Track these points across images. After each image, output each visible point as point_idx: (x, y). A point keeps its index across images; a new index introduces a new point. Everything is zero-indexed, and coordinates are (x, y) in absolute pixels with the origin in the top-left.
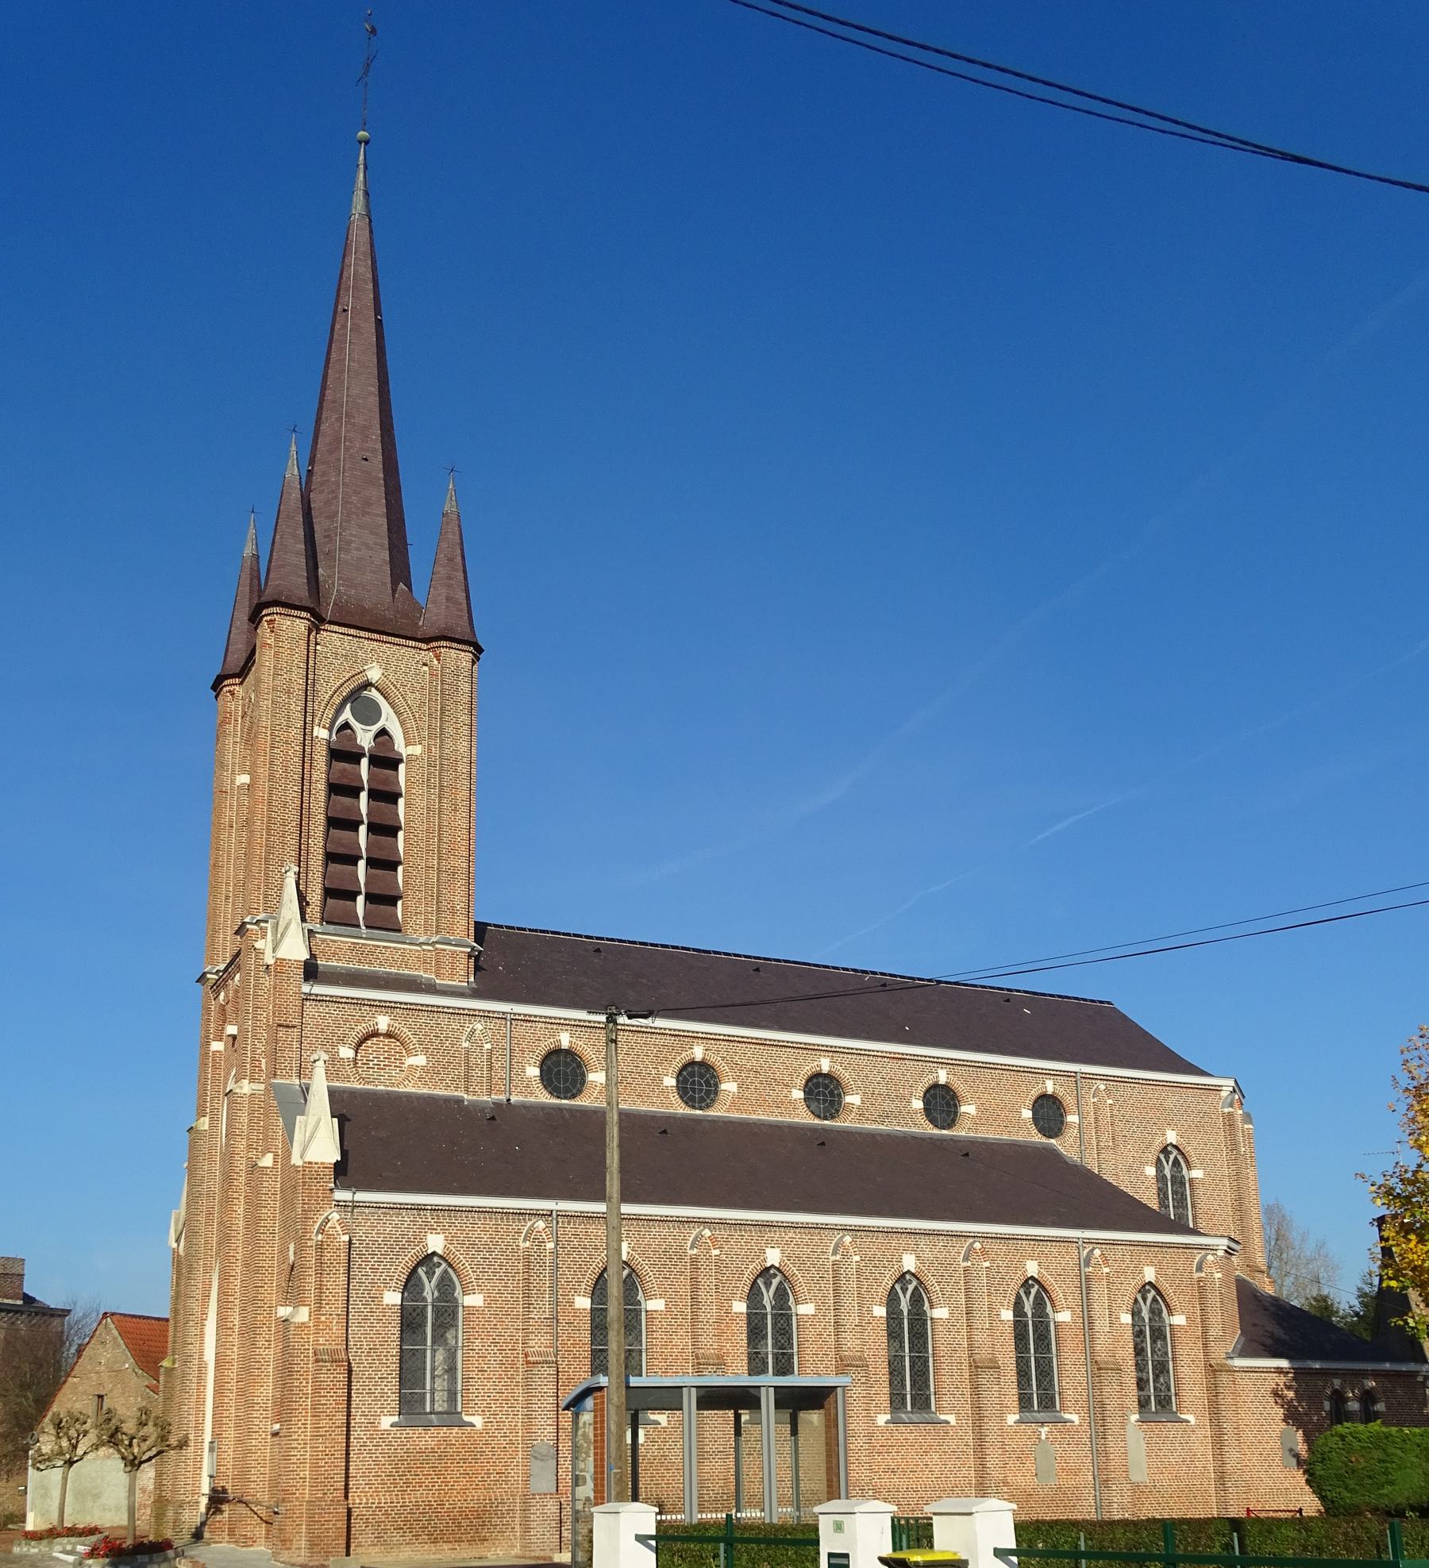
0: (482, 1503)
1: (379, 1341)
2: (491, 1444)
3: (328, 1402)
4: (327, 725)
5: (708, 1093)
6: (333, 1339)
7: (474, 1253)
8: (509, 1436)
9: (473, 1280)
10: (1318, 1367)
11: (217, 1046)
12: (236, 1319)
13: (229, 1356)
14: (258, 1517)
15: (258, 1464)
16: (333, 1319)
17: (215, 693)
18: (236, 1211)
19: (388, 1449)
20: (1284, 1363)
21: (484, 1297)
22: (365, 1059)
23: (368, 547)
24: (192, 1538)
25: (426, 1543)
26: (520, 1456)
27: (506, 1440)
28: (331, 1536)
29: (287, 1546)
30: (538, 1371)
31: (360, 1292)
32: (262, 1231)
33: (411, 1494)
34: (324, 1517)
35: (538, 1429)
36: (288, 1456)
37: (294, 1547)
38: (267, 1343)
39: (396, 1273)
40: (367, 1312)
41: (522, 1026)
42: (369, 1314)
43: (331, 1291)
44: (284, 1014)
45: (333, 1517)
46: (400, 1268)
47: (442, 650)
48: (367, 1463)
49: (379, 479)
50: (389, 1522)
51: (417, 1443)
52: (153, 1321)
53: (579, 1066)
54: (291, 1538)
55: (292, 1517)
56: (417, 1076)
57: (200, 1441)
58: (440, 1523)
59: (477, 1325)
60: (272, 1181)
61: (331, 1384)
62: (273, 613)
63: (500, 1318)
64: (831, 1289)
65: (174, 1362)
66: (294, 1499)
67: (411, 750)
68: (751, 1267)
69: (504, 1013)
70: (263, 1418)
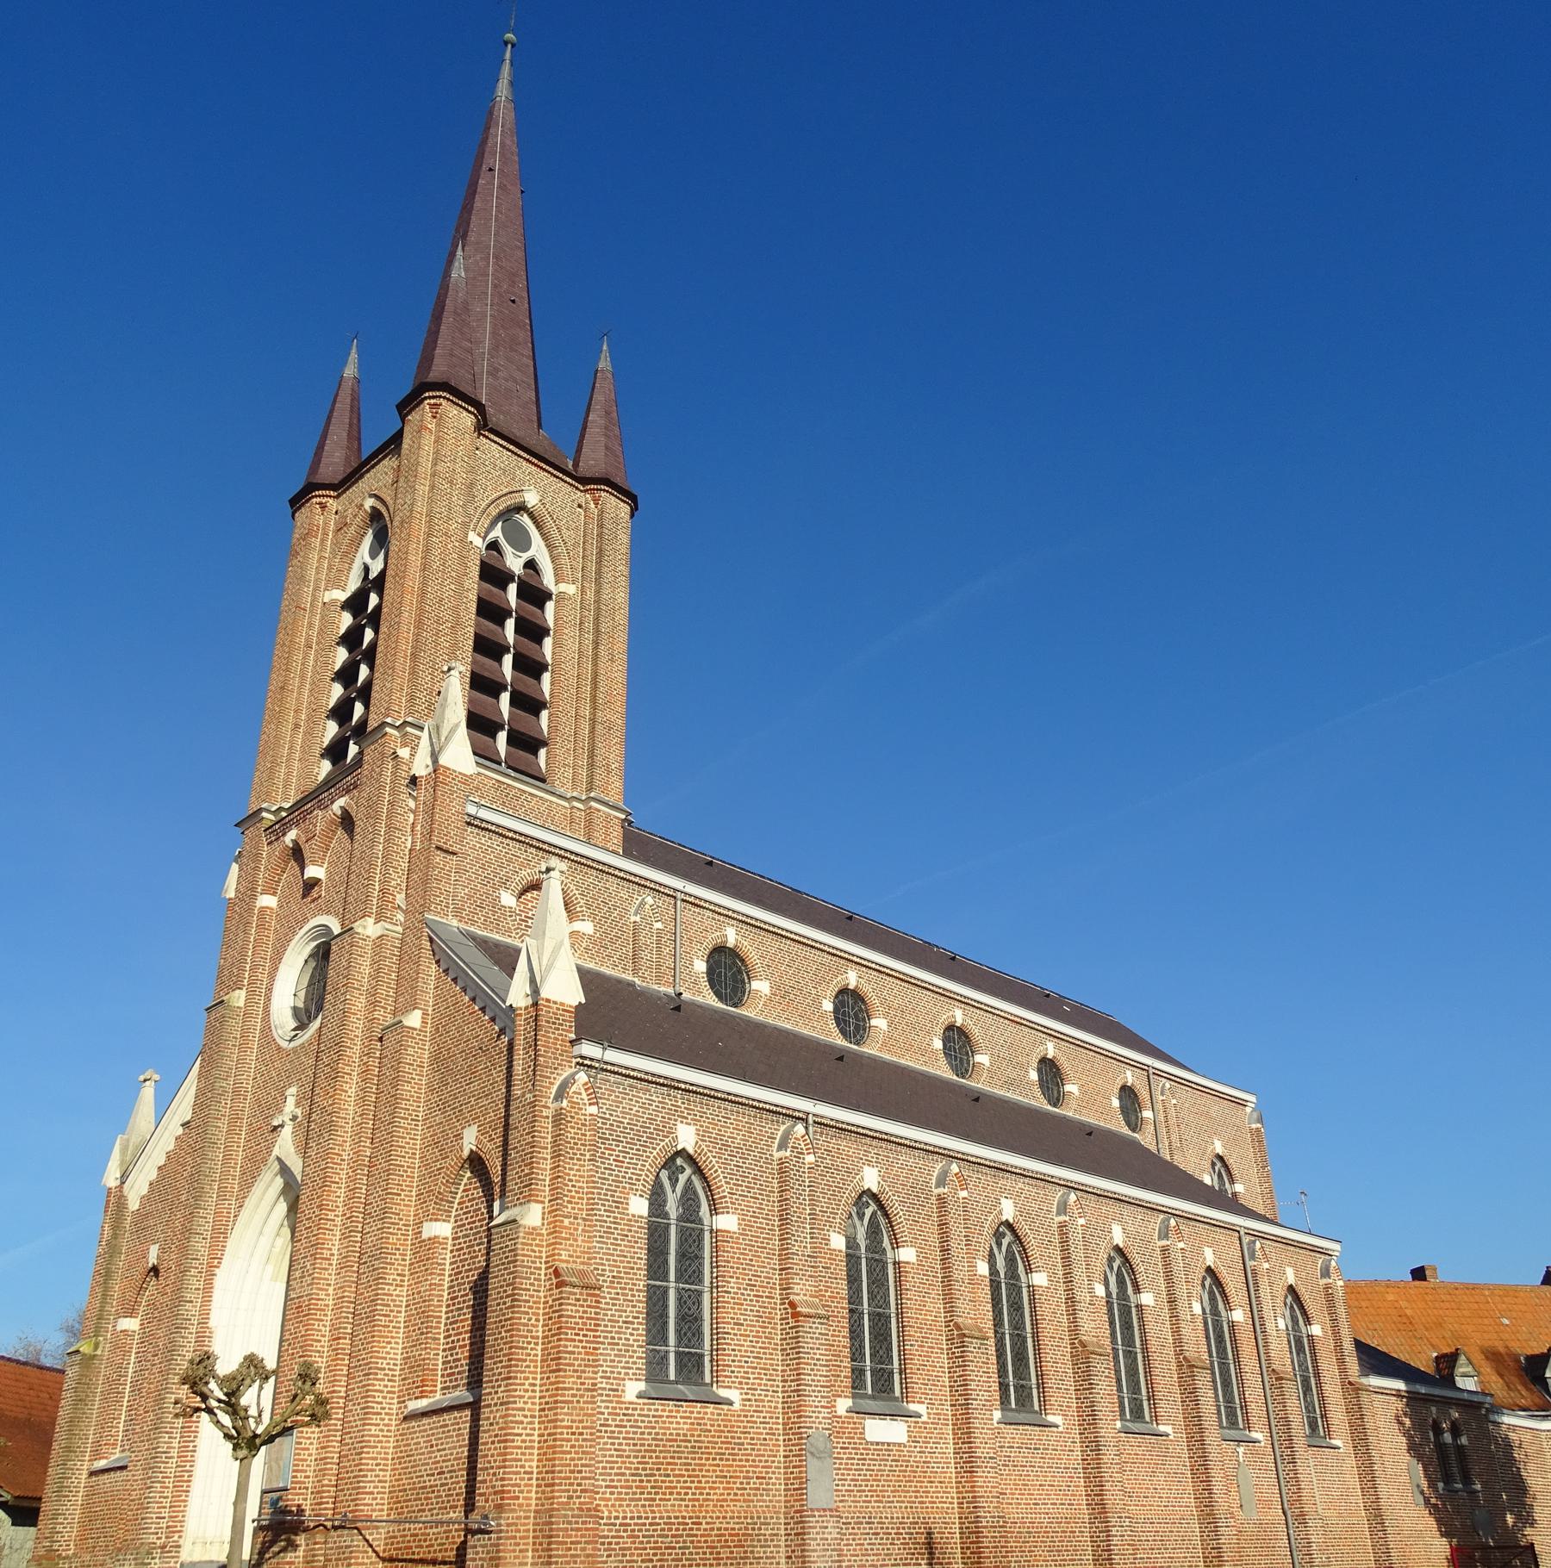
0: (743, 1523)
3: (576, 1350)
6: (579, 1254)
9: (726, 1194)
10: (1423, 1392)
11: (268, 901)
13: (322, 1300)
15: (377, 1465)
20: (1401, 1385)
22: (523, 914)
23: (515, 381)
30: (811, 1327)
34: (571, 1536)
36: (506, 1435)
38: (399, 1278)
42: (613, 1226)
45: (582, 1536)
46: (647, 1164)
47: (603, 494)
48: (608, 1453)
51: (667, 1425)
53: (740, 972)
55: (515, 1537)
57: (191, 1448)
61: (580, 1321)
62: (440, 397)
65: (96, 1347)
67: (563, 587)
68: (990, 1219)
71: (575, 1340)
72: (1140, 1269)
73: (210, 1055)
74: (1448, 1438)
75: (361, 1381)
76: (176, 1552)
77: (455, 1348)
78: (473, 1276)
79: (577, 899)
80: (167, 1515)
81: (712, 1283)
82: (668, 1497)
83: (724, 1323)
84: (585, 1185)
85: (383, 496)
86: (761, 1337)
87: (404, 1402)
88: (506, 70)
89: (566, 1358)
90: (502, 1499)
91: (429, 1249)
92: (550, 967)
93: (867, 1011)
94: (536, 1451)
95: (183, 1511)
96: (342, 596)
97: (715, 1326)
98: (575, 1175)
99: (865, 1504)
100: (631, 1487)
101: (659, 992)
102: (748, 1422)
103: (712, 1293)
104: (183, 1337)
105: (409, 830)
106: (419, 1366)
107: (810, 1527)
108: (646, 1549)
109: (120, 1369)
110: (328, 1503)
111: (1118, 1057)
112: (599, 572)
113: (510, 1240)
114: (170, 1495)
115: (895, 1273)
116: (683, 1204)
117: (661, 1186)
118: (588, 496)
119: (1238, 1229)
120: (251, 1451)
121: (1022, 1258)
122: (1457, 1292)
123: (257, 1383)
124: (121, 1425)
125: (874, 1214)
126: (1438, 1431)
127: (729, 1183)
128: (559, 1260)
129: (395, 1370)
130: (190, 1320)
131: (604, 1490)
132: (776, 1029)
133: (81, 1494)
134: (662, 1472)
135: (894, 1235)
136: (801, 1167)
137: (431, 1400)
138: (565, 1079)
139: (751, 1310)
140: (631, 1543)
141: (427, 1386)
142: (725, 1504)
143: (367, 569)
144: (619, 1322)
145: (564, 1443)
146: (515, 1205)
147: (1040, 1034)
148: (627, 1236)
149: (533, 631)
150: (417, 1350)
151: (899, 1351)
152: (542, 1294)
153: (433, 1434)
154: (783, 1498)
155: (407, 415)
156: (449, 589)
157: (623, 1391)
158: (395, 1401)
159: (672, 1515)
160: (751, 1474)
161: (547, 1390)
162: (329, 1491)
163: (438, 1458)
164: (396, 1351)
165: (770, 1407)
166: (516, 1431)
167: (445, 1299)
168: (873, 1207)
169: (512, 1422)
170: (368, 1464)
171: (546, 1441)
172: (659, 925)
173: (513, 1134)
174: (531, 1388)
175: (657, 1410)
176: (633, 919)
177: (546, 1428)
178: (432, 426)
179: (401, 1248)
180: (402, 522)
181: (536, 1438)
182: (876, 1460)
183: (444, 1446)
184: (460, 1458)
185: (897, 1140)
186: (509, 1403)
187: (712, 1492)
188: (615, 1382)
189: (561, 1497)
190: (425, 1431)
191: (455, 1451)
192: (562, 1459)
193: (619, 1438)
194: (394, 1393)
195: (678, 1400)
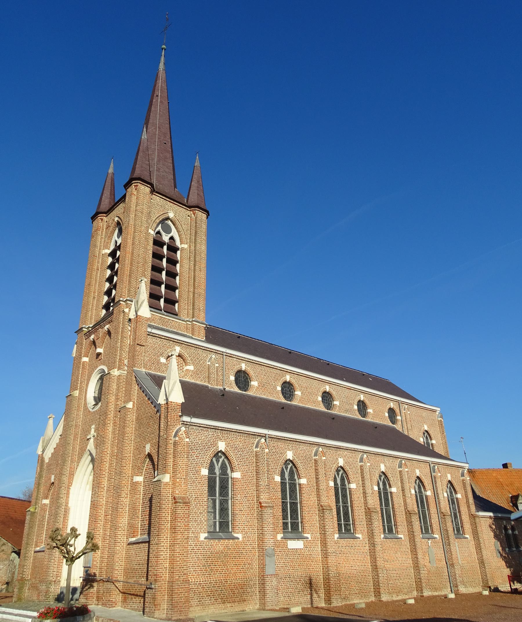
0: (243, 580)
3: (181, 525)
4: (154, 230)
5: (290, 395)
6: (182, 491)
8: (252, 545)
11: (85, 359)
12: (105, 483)
13: (101, 502)
14: (119, 590)
15: (119, 560)
16: (182, 481)
18: (109, 430)
20: (491, 514)
23: (166, 172)
24: (55, 601)
25: (220, 603)
26: (257, 555)
28: (183, 601)
29: (158, 608)
30: (267, 511)
32: (126, 439)
33: (213, 576)
34: (180, 590)
36: (158, 555)
37: (161, 608)
38: (126, 495)
39: (206, 459)
41: (228, 358)
42: (195, 479)
43: (181, 466)
45: (184, 590)
46: (208, 457)
47: (196, 211)
48: (194, 559)
51: (215, 548)
53: (247, 378)
54: (160, 603)
55: (161, 591)
61: (183, 515)
62: (138, 183)
63: (247, 484)
65: (36, 509)
67: (183, 246)
68: (334, 466)
69: (223, 352)
70: (123, 535)
71: (181, 522)
72: (391, 479)
73: (68, 413)
74: (510, 532)
75: (114, 531)
76: (59, 583)
77: (144, 520)
78: (150, 496)
79: (187, 358)
80: (56, 570)
81: (232, 496)
82: (216, 573)
83: (236, 510)
85: (121, 217)
86: (249, 515)
87: (128, 538)
88: (163, 58)
89: (177, 528)
90: (156, 577)
91: (136, 486)
92: (172, 390)
93: (294, 389)
94: (168, 560)
95: (61, 569)
96: (108, 251)
97: (233, 512)
98: (181, 463)
99: (288, 571)
100: (202, 570)
101: (217, 389)
102: (245, 545)
103: (232, 500)
104: (60, 510)
105: (129, 337)
106: (133, 526)
107: (267, 581)
109: (43, 517)
110: (104, 572)
111: (387, 398)
112: (195, 239)
113: (159, 487)
114: (57, 563)
115: (299, 488)
116: (221, 469)
117: (213, 464)
118: (191, 212)
119: (429, 462)
120: (72, 562)
121: (347, 479)
122: (519, 472)
123: (74, 538)
124: (44, 536)
125: (291, 467)
126: (506, 529)
128: (176, 494)
129: (125, 527)
130: (62, 504)
132: (261, 399)
133: (32, 558)
134: (214, 564)
135: (299, 474)
137: (136, 538)
138: (178, 429)
139: (246, 505)
140: (203, 590)
142: (236, 574)
143: (116, 242)
145: (177, 558)
146: (161, 474)
147: (358, 392)
148: (200, 483)
149: (172, 262)
150: (132, 521)
151: (301, 515)
152: (170, 505)
153: (137, 551)
155: (127, 189)
156: (142, 250)
157: (199, 537)
158: (125, 538)
159: (217, 579)
160: (246, 563)
161: (172, 539)
162: (104, 568)
163: (138, 559)
165: (253, 539)
166: (161, 554)
167: (141, 503)
168: (291, 465)
169: (159, 551)
170: (116, 560)
171: (171, 557)
172: (217, 365)
173: (160, 449)
174: (166, 538)
175: (211, 543)
176: (208, 363)
177: (171, 553)
178: (135, 193)
180: (126, 228)
181: (168, 556)
182: (292, 555)
183: (140, 555)
184: (145, 560)
186: (158, 544)
187: (232, 570)
188: (196, 534)
189: (176, 577)
190: (134, 549)
191: (144, 557)
192: (176, 564)
193: (198, 554)
194: (125, 535)
195: (219, 539)
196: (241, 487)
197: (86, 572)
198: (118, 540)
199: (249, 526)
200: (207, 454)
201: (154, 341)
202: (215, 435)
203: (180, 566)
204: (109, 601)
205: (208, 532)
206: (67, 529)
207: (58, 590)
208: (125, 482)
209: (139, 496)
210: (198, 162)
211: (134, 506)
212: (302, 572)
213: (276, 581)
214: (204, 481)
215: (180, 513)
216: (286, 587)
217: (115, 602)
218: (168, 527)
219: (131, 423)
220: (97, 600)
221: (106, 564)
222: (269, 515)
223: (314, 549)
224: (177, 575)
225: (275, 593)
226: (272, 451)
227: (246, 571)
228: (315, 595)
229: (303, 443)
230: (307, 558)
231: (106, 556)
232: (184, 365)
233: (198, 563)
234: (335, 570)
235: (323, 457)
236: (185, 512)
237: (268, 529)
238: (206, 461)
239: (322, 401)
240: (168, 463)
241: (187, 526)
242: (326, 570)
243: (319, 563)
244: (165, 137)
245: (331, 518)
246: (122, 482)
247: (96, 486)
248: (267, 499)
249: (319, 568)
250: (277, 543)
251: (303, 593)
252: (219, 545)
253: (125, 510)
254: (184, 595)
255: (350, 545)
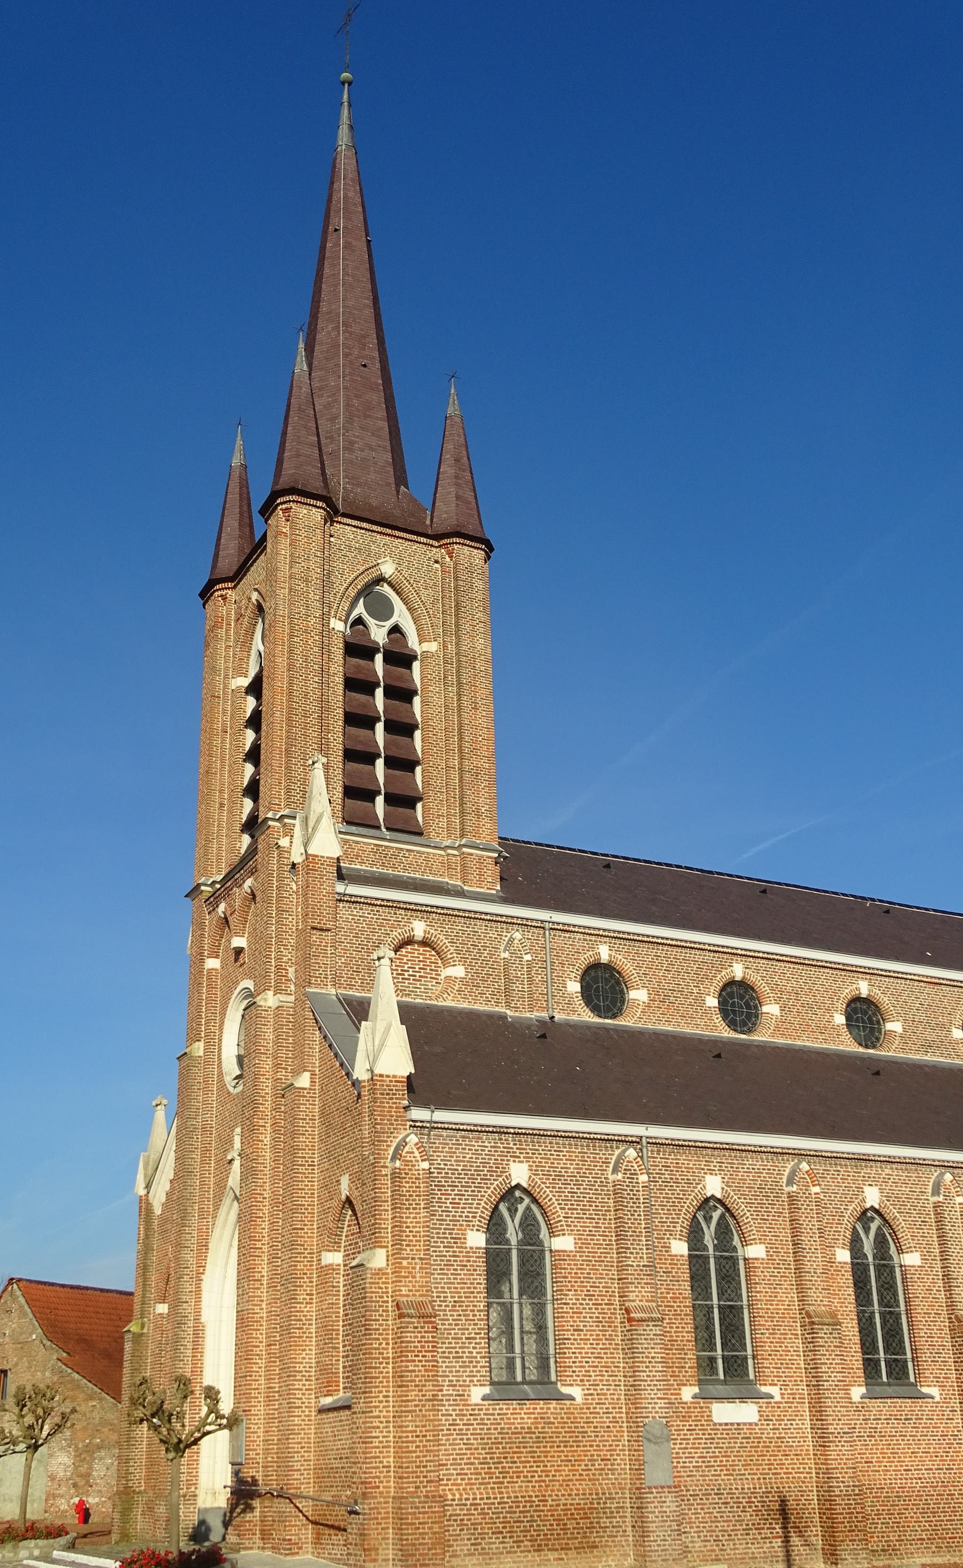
0: (588, 1499)
1: (464, 1293)
2: (593, 1423)
3: (416, 1369)
4: (344, 618)
5: (749, 1016)
6: (418, 1288)
7: (560, 1186)
8: (612, 1413)
9: (561, 1218)
11: (212, 963)
12: (264, 1269)
13: (257, 1313)
14: (304, 1515)
17: (202, 602)
18: (263, 1141)
19: (480, 1429)
21: (575, 1239)
22: (399, 969)
23: (371, 448)
24: (190, 1540)
25: (530, 1551)
26: (626, 1438)
27: (609, 1418)
28: (427, 1544)
29: (373, 1557)
30: (644, 1330)
31: (441, 1231)
32: (300, 1163)
33: (508, 1487)
34: (418, 1518)
35: (649, 1403)
36: (366, 1437)
38: (308, 1297)
39: (478, 1208)
40: (450, 1256)
41: (560, 936)
42: (452, 1259)
43: (411, 1229)
44: (318, 916)
45: (428, 1518)
46: (482, 1203)
47: (455, 547)
48: (457, 1447)
49: (378, 385)
50: (486, 1523)
51: (512, 1421)
52: (58, 1288)
53: (618, 983)
54: (376, 1546)
56: (456, 989)
58: (543, 1526)
59: (569, 1273)
60: (310, 1104)
61: (419, 1345)
62: (290, 501)
63: (593, 1265)
64: (935, 1236)
65: (143, 1327)
66: (378, 1495)
67: (426, 646)
68: (851, 1208)
69: (542, 921)
70: (306, 1390)
71: (414, 1361)
75: (286, 1381)
76: (194, 1500)
80: (185, 1471)
82: (515, 1480)
84: (421, 1229)
91: (326, 1274)
92: (382, 1045)
93: (758, 998)
95: (196, 1468)
96: (245, 682)
98: (412, 1222)
100: (480, 1474)
101: (531, 1019)
104: (183, 1331)
108: (495, 1523)
112: (457, 625)
113: (362, 1279)
117: (501, 1218)
121: (893, 1240)
125: (722, 1217)
127: (563, 1209)
128: (400, 1295)
130: (187, 1317)
131: (455, 1477)
132: (657, 1035)
133: (145, 1443)
134: (509, 1460)
136: (634, 1187)
137: (335, 1398)
141: (331, 1386)
142: (570, 1483)
144: (462, 1339)
145: (410, 1444)
148: (466, 1266)
154: (628, 1476)
156: (314, 681)
157: (469, 1395)
158: (313, 1396)
161: (397, 1401)
162: (273, 1466)
164: (311, 1356)
166: (374, 1434)
167: (341, 1315)
168: (720, 1210)
169: (369, 1427)
170: (294, 1448)
171: (397, 1442)
172: (528, 957)
174: (384, 1399)
179: (308, 1272)
181: (391, 1439)
182: (725, 1439)
185: (740, 1148)
187: (557, 1474)
188: (460, 1388)
189: (409, 1487)
193: (467, 1434)
194: (311, 1390)
196: (576, 1273)
197: (236, 1473)
198: (296, 1401)
199: (601, 1367)
200: (481, 1196)
201: (355, 913)
202: (500, 1147)
203: (418, 1464)
204: (284, 1540)
205: (492, 1383)
206: (202, 1375)
207: (193, 1516)
208: (304, 1266)
209: (334, 1298)
210: (456, 402)
211: (326, 1321)
212: (756, 1481)
213: (673, 1501)
214: (475, 1262)
215: (413, 1340)
216: (710, 1517)
217: (298, 1543)
218: (388, 1372)
219: (309, 1123)
220: (263, 1539)
221: (275, 1456)
222: (651, 1339)
223: (791, 1424)
224: (412, 1482)
225: (671, 1531)
226: (660, 1178)
227: (597, 1477)
228: (795, 1540)
229: (752, 1152)
230: (769, 1447)
231: (276, 1438)
232: (440, 965)
233: (469, 1456)
234: (849, 1477)
235: (813, 1185)
236: (424, 1337)
237: (648, 1376)
238: (480, 1213)
239: (847, 1025)
240: (381, 1224)
241: (431, 1371)
242: (823, 1478)
243: (806, 1461)
244: (363, 346)
245: (835, 1346)
246: (296, 1266)
247: (245, 1275)
248: (647, 1301)
249: (808, 1473)
250: (681, 1409)
251: (760, 1534)
252: (520, 1414)
253: (309, 1333)
254: (429, 1528)
255: (901, 1415)
